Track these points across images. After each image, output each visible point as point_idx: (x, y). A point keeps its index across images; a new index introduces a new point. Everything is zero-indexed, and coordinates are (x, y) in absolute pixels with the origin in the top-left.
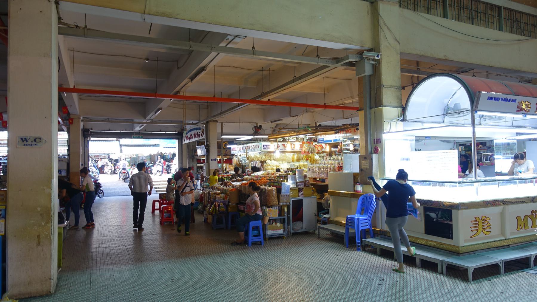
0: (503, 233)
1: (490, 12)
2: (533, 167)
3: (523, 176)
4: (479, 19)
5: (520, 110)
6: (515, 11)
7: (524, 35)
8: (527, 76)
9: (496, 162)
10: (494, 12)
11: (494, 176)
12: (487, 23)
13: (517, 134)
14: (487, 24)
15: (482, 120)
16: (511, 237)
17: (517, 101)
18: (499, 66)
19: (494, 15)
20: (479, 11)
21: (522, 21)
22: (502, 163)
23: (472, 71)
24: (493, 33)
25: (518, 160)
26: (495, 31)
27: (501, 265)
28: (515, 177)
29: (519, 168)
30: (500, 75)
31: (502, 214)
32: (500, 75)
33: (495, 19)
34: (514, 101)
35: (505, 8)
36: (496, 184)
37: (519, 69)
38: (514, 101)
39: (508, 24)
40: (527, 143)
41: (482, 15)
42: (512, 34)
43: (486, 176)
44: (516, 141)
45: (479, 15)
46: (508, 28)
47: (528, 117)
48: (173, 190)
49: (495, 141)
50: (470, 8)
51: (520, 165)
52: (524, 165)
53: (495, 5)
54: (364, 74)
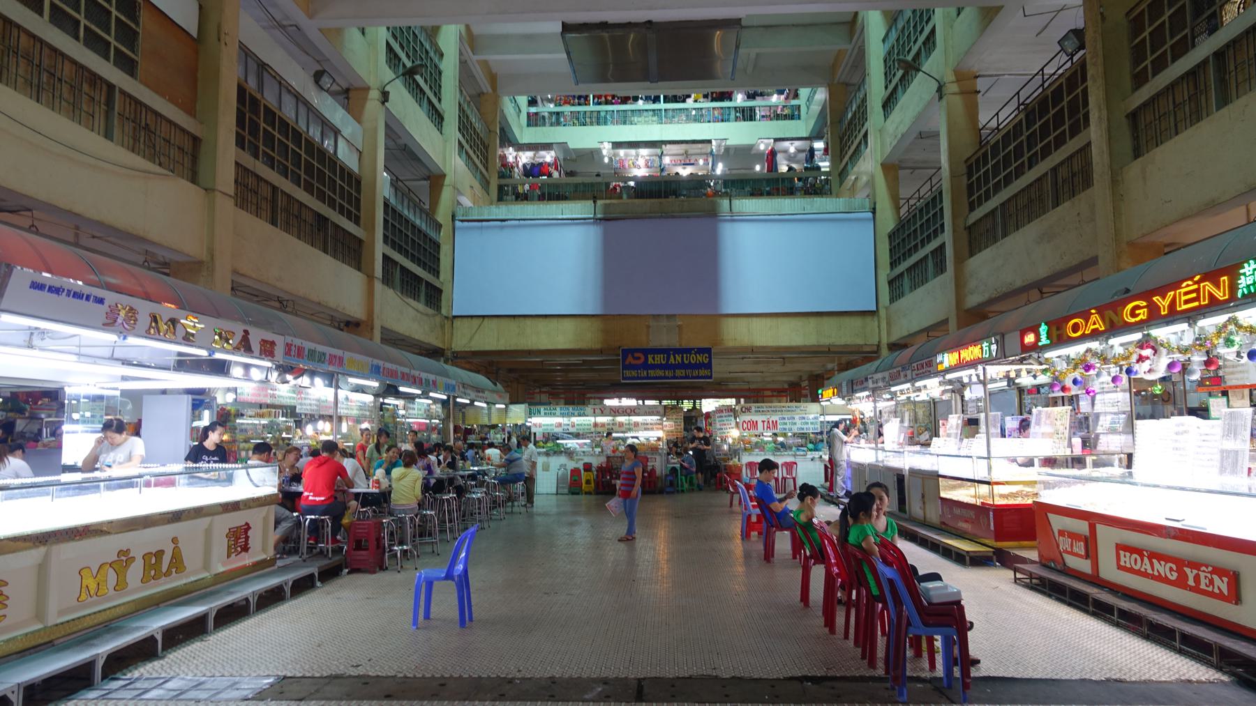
0: (39, 615)
1: (86, 87)
2: (143, 453)
3: (115, 472)
4: (57, 94)
5: (109, 324)
6: (146, 106)
7: (160, 165)
8: (162, 255)
9: (66, 439)
10: (98, 92)
11: (58, 474)
12: (77, 112)
13: (124, 378)
14: (74, 111)
15: (34, 337)
16: (59, 621)
17: (107, 303)
18: (96, 218)
19: (97, 98)
20: (58, 74)
21: (158, 133)
22: (77, 442)
23: (29, 214)
24: (92, 140)
25: (109, 434)
26: (94, 135)
27: (13, 698)
28: (97, 474)
29: (112, 454)
30: (99, 238)
31: (42, 569)
32: (99, 238)
33: (97, 108)
34: (101, 301)
35: (123, 92)
36: (48, 494)
37: (141, 234)
38: (101, 301)
39: (126, 129)
40: (146, 398)
41: (65, 89)
42: (133, 155)
43: (36, 475)
44: (118, 393)
45: (57, 85)
46: (126, 139)
47: (132, 340)
48: (382, 407)
49: (68, 391)
50: (36, 61)
51: (114, 446)
52: (120, 448)
53: (101, 78)
54: (608, 201)
